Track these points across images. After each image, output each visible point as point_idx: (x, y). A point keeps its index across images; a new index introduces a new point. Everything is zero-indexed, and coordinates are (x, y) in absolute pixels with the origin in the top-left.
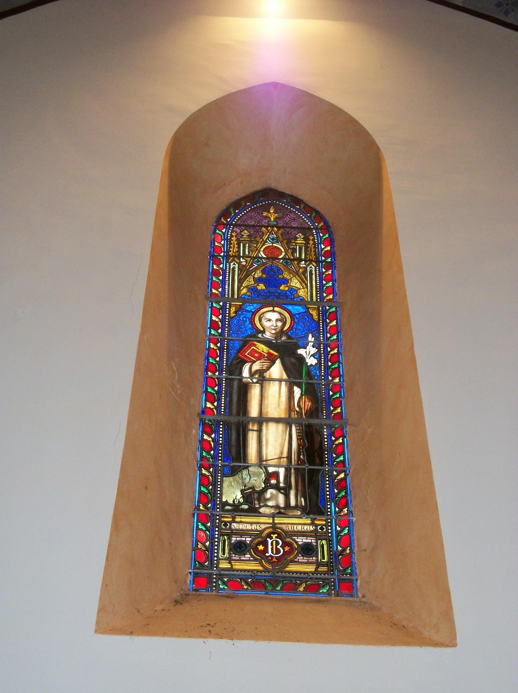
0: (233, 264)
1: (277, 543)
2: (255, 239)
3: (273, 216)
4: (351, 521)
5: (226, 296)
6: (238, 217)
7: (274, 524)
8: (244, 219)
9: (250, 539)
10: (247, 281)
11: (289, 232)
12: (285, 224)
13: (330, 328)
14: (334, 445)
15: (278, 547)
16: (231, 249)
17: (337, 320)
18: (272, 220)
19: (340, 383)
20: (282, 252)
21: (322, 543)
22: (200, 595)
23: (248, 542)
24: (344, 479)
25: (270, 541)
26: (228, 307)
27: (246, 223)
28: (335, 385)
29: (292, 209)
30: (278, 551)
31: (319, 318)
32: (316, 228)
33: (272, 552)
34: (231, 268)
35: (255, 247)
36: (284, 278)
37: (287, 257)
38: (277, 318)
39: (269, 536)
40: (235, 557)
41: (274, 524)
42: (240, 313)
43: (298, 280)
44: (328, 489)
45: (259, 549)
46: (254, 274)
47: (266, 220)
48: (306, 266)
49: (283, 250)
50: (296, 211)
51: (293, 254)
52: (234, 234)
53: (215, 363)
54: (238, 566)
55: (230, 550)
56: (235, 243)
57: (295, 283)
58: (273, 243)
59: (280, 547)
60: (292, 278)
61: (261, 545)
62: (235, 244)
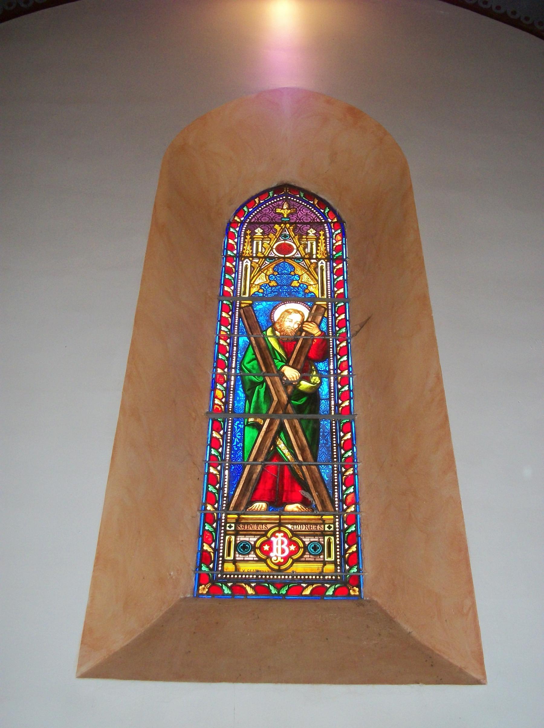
1: (283, 543)
2: (268, 236)
7: (280, 519)
8: (258, 217)
12: (298, 220)
14: (344, 459)
18: (285, 216)
40: (239, 557)
41: (280, 519)
48: (317, 261)
50: (307, 205)
51: (304, 249)
55: (235, 550)
57: (305, 278)
60: (303, 274)
62: (249, 242)
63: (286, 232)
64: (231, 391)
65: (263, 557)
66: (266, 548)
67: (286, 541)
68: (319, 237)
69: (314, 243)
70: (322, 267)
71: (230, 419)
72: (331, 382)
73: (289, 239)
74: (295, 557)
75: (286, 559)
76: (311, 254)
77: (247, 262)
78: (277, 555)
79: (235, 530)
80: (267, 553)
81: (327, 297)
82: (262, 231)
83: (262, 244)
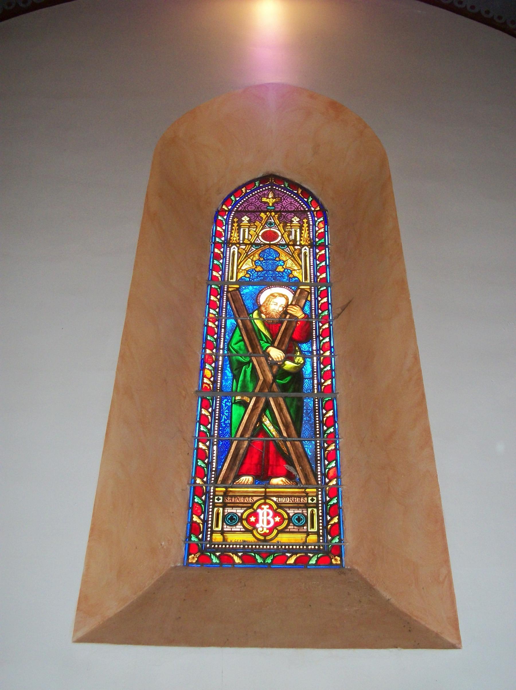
1: (268, 514)
2: (254, 224)
5: (209, 539)
7: (265, 492)
8: (245, 206)
12: (283, 209)
14: (326, 435)
18: (271, 205)
40: (227, 528)
41: (265, 492)
48: (300, 248)
50: (291, 194)
51: (289, 236)
55: (223, 521)
57: (290, 263)
60: (287, 260)
62: (236, 230)
63: (272, 220)
64: (220, 370)
65: (250, 528)
66: (253, 519)
67: (271, 513)
68: (303, 224)
69: (298, 230)
70: (305, 253)
71: (219, 397)
72: (314, 362)
73: (275, 226)
74: (280, 528)
75: (271, 530)
76: (295, 240)
77: (234, 248)
78: (262, 526)
79: (223, 502)
80: (253, 524)
81: (311, 281)
82: (248, 219)
83: (249, 231)
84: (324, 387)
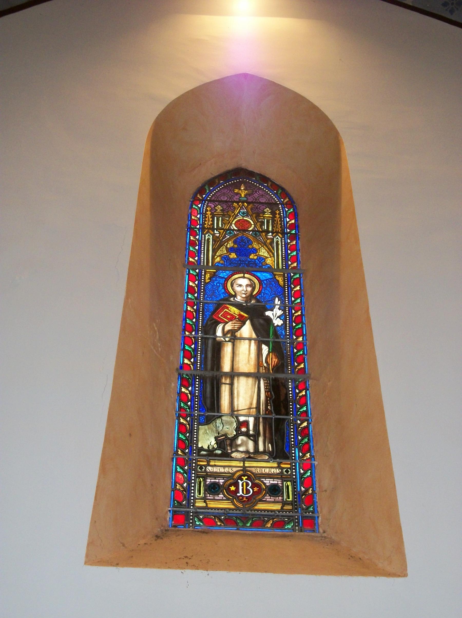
0: (208, 235)
1: (247, 484)
2: (227, 213)
3: (243, 193)
4: (313, 465)
5: (202, 264)
6: (212, 194)
7: (244, 467)
8: (218, 196)
9: (223, 481)
10: (221, 250)
11: (258, 207)
12: (254, 200)
13: (294, 292)
14: (298, 397)
15: (248, 488)
16: (206, 222)
17: (300, 285)
18: (243, 196)
19: (303, 342)
20: (252, 225)
21: (288, 484)
22: (178, 531)
23: (221, 483)
24: (307, 428)
25: (241, 483)
26: (203, 274)
27: (219, 199)
28: (299, 343)
29: (260, 186)
30: (248, 491)
31: (284, 283)
32: (282, 204)
33: (243, 492)
34: (206, 239)
35: (228, 220)
36: (253, 248)
37: (256, 229)
38: (247, 284)
39: (240, 478)
40: (210, 497)
41: (244, 467)
42: (214, 279)
43: (266, 250)
44: (292, 436)
45: (231, 490)
46: (227, 245)
47: (237, 196)
48: (273, 237)
49: (252, 223)
50: (264, 188)
51: (261, 226)
52: (208, 209)
53: (192, 324)
54: (212, 505)
55: (205, 490)
56: (210, 217)
57: (263, 252)
58: (243, 217)
59: (250, 488)
60: (260, 248)
61: (233, 486)
62: (210, 218)
77: (209, 236)
84: (290, 256)
